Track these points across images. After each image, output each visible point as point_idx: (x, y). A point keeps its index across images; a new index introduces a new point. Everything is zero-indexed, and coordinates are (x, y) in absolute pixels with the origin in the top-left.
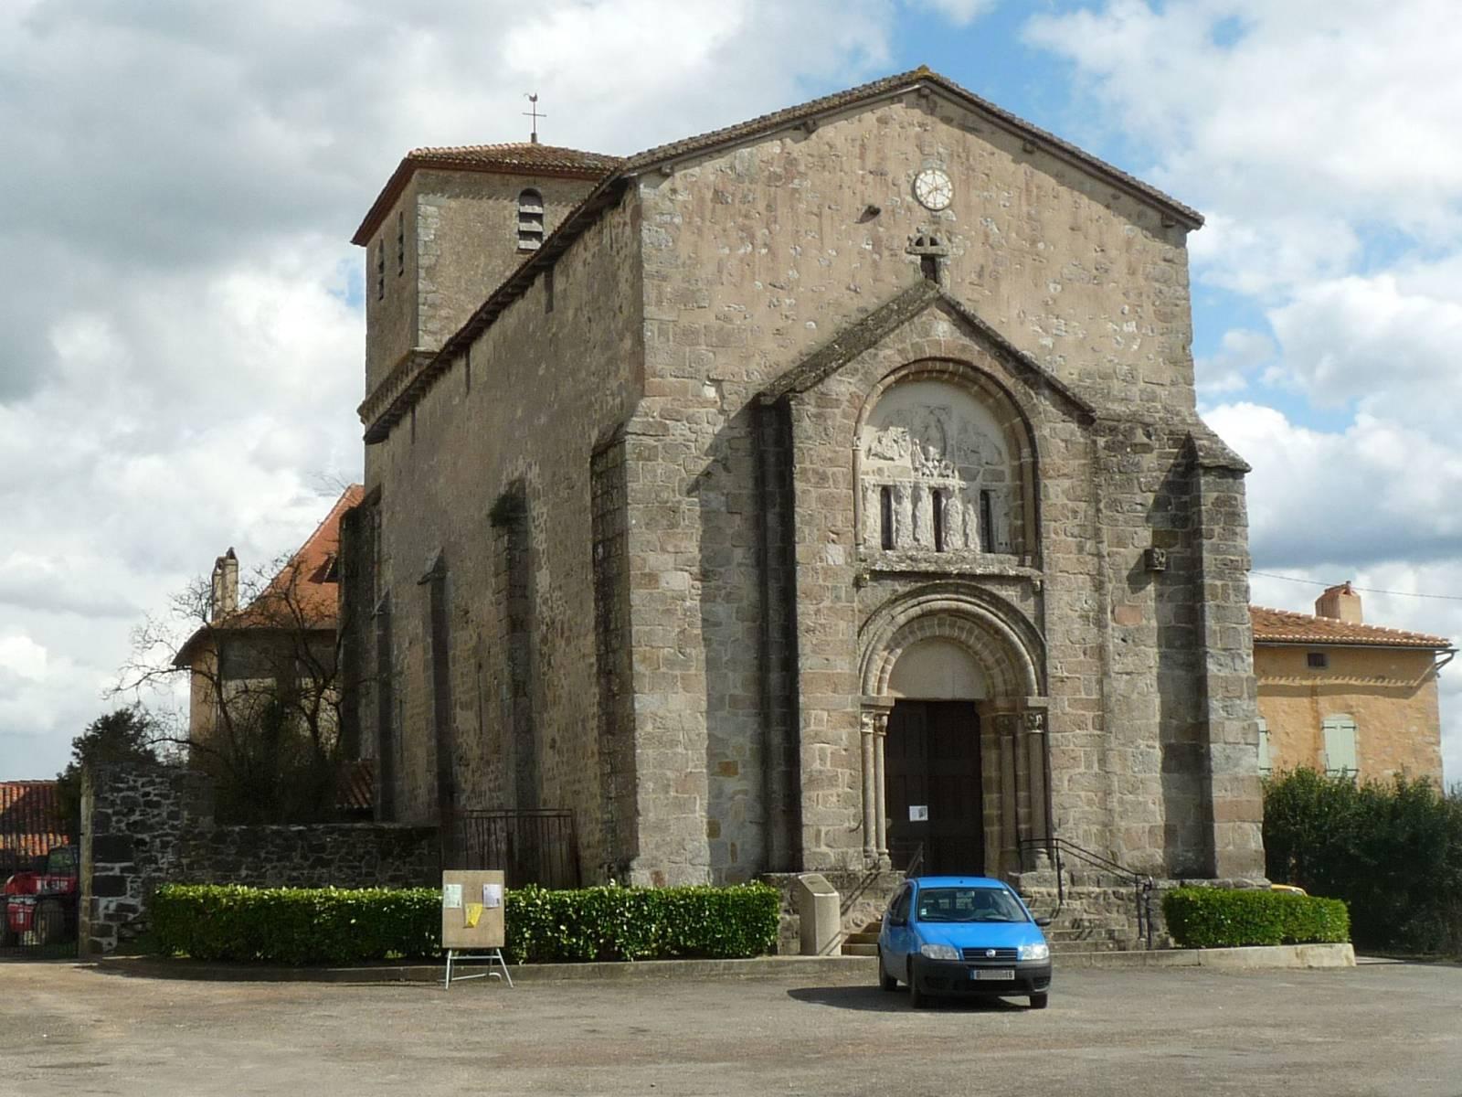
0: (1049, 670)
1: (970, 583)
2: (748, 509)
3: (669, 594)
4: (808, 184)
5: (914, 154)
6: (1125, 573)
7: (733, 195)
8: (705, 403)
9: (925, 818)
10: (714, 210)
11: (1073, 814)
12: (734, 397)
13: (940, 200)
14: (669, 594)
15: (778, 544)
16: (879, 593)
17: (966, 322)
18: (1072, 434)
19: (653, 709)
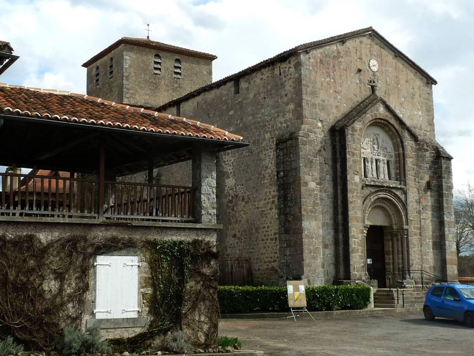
0: (409, 218)
1: (389, 189)
2: (330, 163)
3: (311, 189)
4: (343, 60)
5: (369, 54)
6: (423, 188)
7: (325, 61)
8: (318, 128)
9: (371, 263)
10: (320, 66)
11: (415, 262)
12: (326, 127)
13: (375, 69)
14: (311, 189)
15: (340, 175)
16: (367, 191)
17: (388, 108)
18: (413, 145)
19: (307, 226)
